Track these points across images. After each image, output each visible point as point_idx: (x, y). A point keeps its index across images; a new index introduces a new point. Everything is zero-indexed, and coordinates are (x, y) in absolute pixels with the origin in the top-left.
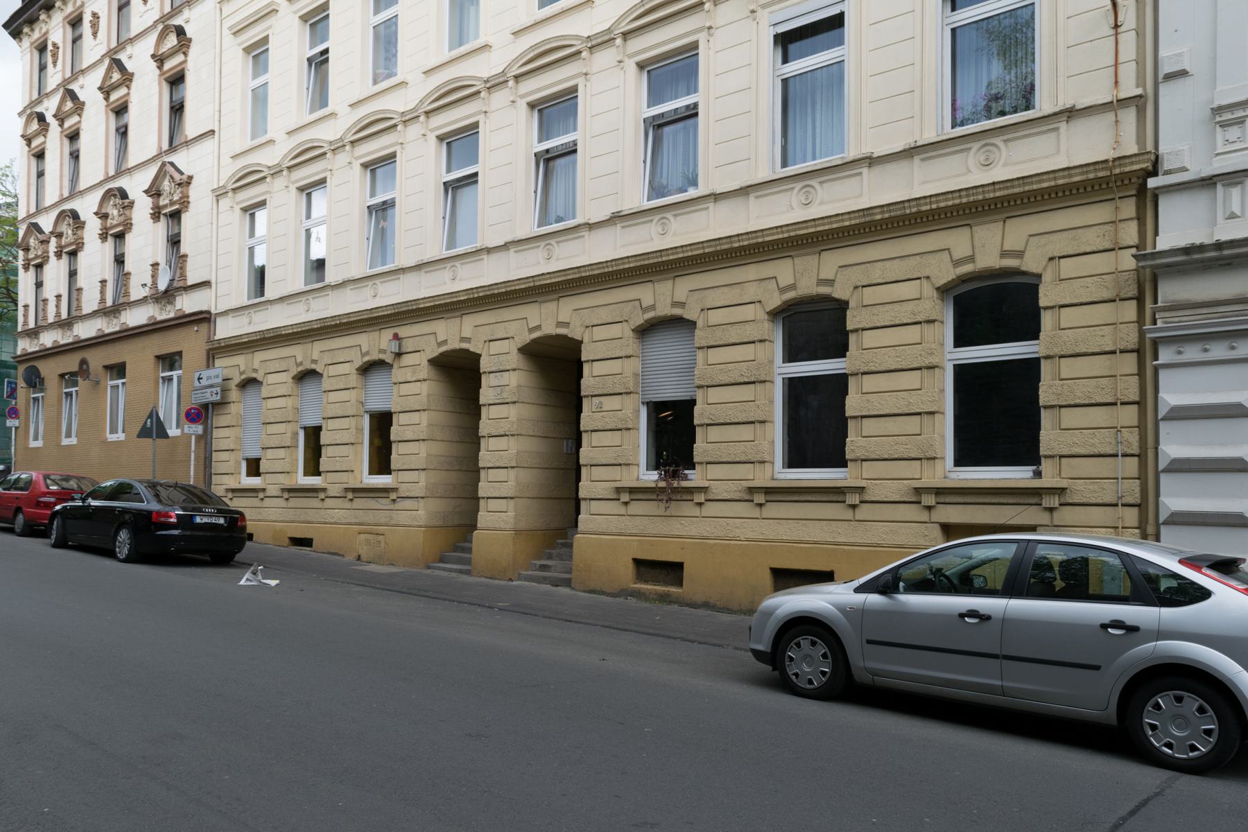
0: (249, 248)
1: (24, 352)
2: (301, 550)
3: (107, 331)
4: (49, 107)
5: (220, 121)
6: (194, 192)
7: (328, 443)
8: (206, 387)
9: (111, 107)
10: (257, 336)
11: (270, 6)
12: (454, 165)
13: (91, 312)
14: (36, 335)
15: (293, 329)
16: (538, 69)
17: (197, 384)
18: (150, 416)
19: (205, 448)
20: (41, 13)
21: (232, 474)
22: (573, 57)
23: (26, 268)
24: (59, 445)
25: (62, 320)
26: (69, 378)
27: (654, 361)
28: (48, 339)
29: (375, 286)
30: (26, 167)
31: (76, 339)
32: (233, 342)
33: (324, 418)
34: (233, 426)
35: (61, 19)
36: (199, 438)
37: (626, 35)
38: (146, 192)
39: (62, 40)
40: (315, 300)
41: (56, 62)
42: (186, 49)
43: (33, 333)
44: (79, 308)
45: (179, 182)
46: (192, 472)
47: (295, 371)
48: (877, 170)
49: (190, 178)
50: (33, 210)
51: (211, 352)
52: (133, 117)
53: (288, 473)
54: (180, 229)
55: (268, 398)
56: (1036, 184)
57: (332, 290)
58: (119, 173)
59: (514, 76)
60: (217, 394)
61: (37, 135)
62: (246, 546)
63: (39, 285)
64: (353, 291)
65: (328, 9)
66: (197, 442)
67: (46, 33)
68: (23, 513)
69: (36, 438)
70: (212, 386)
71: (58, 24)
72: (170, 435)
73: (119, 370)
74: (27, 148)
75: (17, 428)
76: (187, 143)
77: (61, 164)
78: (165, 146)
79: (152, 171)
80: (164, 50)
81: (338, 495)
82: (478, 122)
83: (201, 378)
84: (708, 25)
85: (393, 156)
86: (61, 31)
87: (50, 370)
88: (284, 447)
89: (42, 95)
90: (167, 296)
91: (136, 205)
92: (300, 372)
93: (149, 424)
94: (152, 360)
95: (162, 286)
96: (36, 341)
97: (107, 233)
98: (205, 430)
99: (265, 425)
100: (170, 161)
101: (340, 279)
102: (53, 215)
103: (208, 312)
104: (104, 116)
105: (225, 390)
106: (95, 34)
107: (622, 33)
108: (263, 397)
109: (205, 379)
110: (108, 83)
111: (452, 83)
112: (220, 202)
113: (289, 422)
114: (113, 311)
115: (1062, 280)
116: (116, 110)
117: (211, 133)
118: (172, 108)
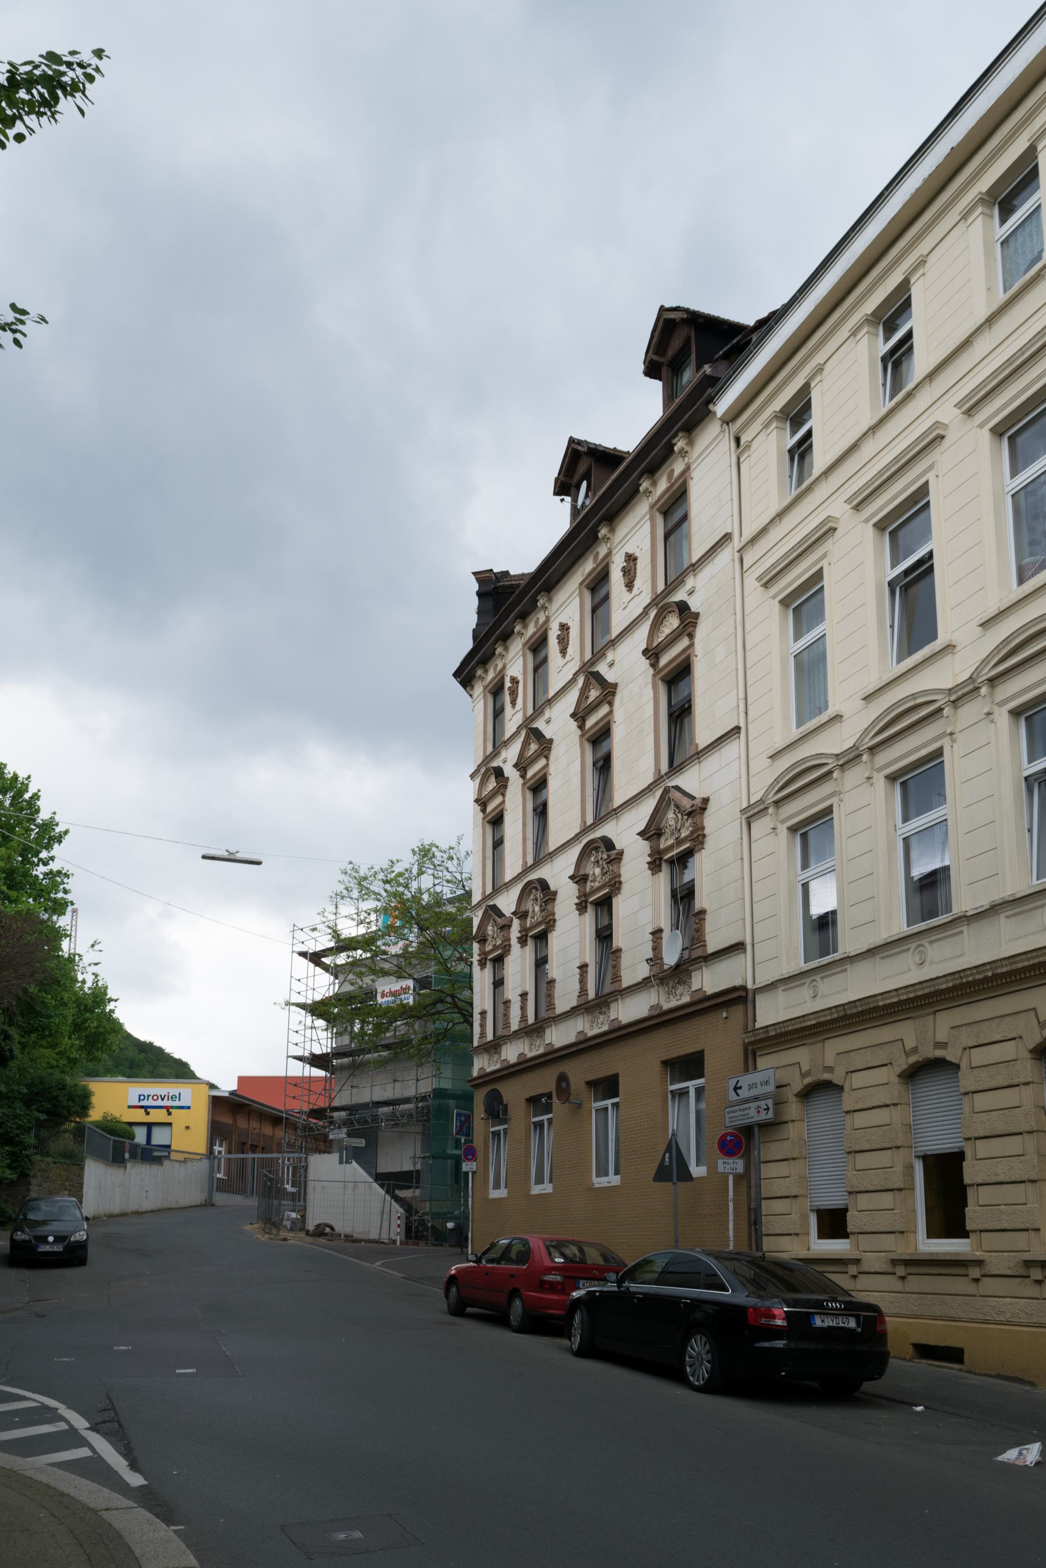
0: (904, 839)
1: (482, 1073)
2: (941, 1367)
3: (591, 1033)
4: (510, 756)
5: (746, 713)
6: (710, 822)
7: (981, 1181)
8: (747, 1101)
9: (587, 736)
10: (831, 1014)
11: (826, 524)
12: (912, 810)
13: (569, 1009)
14: (496, 1049)
15: (899, 995)
16: (922, 720)
17: (732, 1096)
18: (669, 1149)
19: (749, 1195)
20: (496, 646)
21: (797, 1234)
22: (933, 716)
23: (482, 964)
24: (527, 1194)
25: (589, 1002)
26: (538, 1103)
27: (828, 1125)
28: (511, 1053)
29: (921, 949)
30: (481, 839)
31: (549, 1049)
32: (790, 1028)
33: (967, 1139)
34: (794, 1159)
35: (520, 646)
36: (738, 1178)
37: (992, 681)
38: (641, 834)
39: (522, 671)
40: (935, 945)
41: (515, 701)
42: (692, 628)
43: (493, 1047)
44: (551, 1006)
45: (690, 810)
46: (731, 1232)
47: (903, 1063)
48: (975, 926)
49: (706, 801)
50: (489, 890)
51: (750, 1048)
52: (554, 791)
53: (902, 1232)
54: (611, 919)
55: (854, 1111)
56: (822, 1017)
57: (968, 925)
58: (497, 890)
59: (868, 748)
60: (768, 1109)
61: (493, 796)
62: (889, 1364)
63: (498, 983)
64: (1012, 920)
65: (927, 494)
66: (735, 1185)
67: (504, 667)
68: (521, 1299)
69: (497, 1186)
70: (756, 1098)
71: (518, 653)
72: (694, 1176)
73: (608, 1086)
74: (481, 815)
75: (474, 1173)
76: (700, 755)
77: (524, 825)
78: (664, 767)
79: (648, 806)
80: (660, 640)
81: (1009, 1272)
82: (831, 806)
83: (740, 1088)
84: (949, 731)
85: (829, 810)
86: (520, 662)
87: (514, 1093)
88: (892, 1190)
89: (499, 745)
90: (681, 972)
91: (625, 856)
92: (911, 1066)
93: (667, 1160)
94: (657, 1067)
95: (670, 958)
96: (496, 1057)
97: (586, 901)
98: (747, 1167)
99: (851, 1156)
100: (674, 784)
101: (984, 902)
102: (515, 891)
103: (743, 988)
104: (579, 750)
105: (779, 1103)
106: (563, 652)
107: (988, 680)
108: (846, 1110)
109: (745, 1088)
110: (583, 706)
111: (797, 767)
112: (752, 825)
113: (898, 1147)
114: (533, 1031)
115: (973, 1068)
116: (593, 739)
117: (736, 731)
118: (670, 715)
